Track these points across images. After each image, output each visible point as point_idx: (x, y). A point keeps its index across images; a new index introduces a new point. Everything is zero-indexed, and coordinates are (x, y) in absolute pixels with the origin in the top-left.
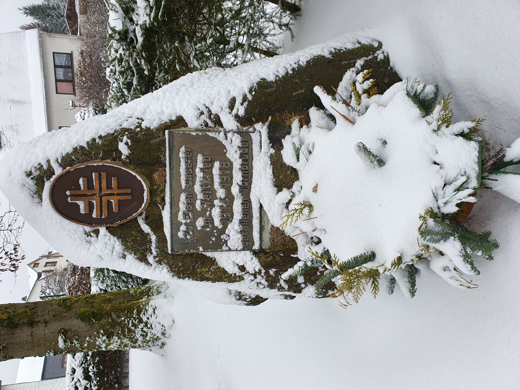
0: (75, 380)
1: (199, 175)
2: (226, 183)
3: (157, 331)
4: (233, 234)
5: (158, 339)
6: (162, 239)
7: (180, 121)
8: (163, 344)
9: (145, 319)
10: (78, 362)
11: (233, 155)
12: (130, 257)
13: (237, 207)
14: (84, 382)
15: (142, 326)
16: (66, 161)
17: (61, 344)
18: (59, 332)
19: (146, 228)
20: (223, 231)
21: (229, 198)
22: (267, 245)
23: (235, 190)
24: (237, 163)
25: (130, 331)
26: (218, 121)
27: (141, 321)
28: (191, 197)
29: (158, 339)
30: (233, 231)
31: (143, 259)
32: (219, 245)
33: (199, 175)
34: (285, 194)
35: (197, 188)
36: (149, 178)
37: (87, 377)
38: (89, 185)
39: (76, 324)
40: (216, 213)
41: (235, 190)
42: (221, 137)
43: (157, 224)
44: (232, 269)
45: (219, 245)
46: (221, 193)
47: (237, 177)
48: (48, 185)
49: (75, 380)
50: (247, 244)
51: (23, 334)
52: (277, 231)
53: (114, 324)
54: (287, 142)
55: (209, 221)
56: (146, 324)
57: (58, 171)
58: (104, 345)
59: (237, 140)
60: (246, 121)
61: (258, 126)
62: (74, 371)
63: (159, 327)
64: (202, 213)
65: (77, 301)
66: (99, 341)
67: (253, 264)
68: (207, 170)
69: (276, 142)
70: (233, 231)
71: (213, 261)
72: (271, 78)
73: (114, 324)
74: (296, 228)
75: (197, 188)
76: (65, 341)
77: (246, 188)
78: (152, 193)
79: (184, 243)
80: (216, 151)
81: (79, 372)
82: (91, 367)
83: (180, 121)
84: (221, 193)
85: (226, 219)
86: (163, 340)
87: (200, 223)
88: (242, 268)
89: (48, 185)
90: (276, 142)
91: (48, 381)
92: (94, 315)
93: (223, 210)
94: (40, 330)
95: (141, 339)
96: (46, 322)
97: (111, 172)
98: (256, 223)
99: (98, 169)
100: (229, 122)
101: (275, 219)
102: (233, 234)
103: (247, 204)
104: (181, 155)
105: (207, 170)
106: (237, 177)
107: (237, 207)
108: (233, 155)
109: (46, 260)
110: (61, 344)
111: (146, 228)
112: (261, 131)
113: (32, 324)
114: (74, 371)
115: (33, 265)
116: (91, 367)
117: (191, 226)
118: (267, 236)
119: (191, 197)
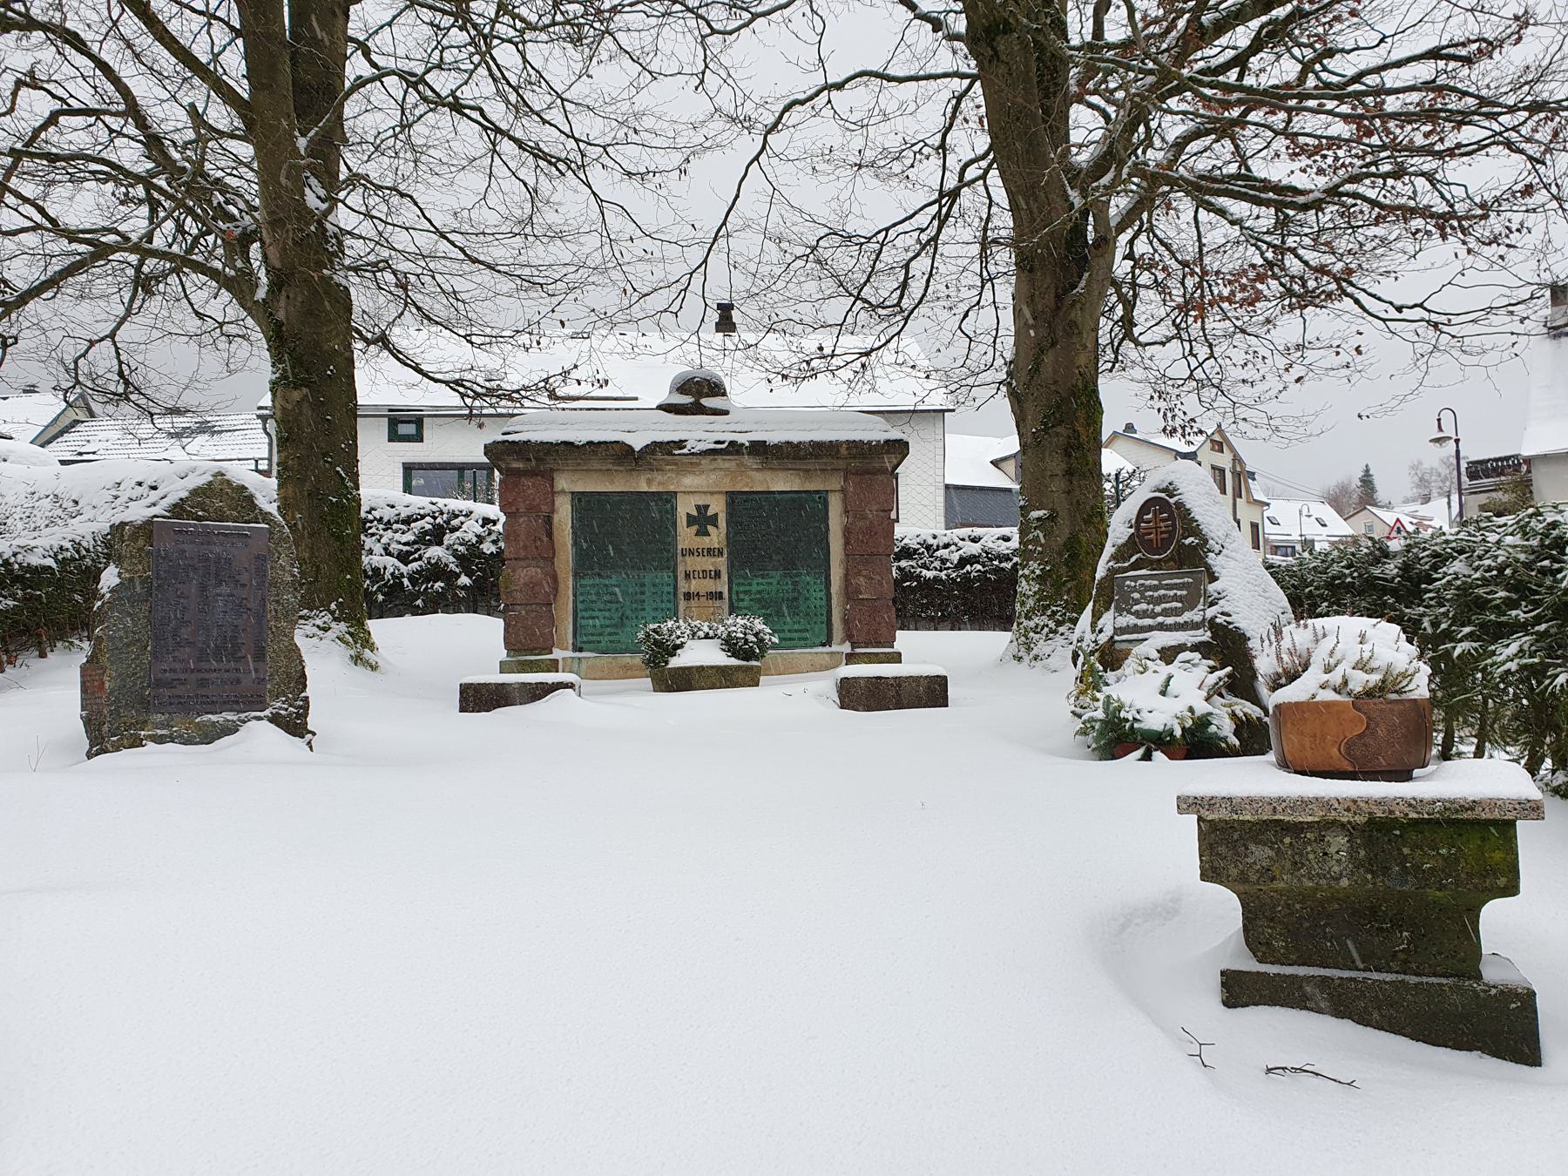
0: (961, 543)
1: (1172, 593)
2: (1165, 613)
3: (1042, 647)
4: (1127, 620)
5: (1029, 649)
6: (1126, 570)
7: (1213, 578)
8: (1020, 659)
9: (1061, 629)
10: (991, 545)
11: (1187, 617)
12: (1113, 550)
13: (1148, 622)
14: (955, 557)
15: (1052, 624)
16: (1179, 505)
17: (1035, 514)
18: (1053, 510)
19: (1133, 559)
20: (1129, 612)
21: (1154, 615)
22: (1117, 646)
23: (1160, 619)
24: (1180, 620)
25: (1046, 607)
26: (1212, 604)
27: (1059, 624)
28: (1155, 588)
29: (1029, 649)
30: (1131, 620)
31: (1114, 557)
32: (1119, 611)
33: (1172, 593)
34: (1156, 655)
35: (1162, 592)
36: (1166, 561)
37: (963, 562)
38: (1163, 520)
39: (1063, 533)
40: (1144, 606)
41: (1160, 619)
42: (1200, 607)
43: (1134, 567)
44: (1100, 624)
45: (1119, 611)
46: (1158, 609)
47: (1170, 620)
48: (1163, 495)
49: (961, 543)
50: (1119, 631)
51: (1056, 464)
52: (1127, 654)
53: (1058, 586)
54: (1197, 655)
55: (1137, 602)
56: (1055, 632)
57: (1172, 501)
58: (1026, 572)
59: (1198, 618)
60: (1212, 624)
61: (1209, 633)
62: (975, 540)
63: (1047, 650)
64: (1143, 597)
65: (1098, 530)
66: (1033, 565)
67: (1103, 639)
68: (1175, 598)
69: (1195, 648)
70: (1131, 620)
71: (1107, 609)
72: (1250, 644)
73: (1058, 586)
74: (1130, 665)
75: (1162, 592)
76: (1038, 519)
77: (1162, 627)
78: (1159, 561)
79: (1121, 586)
80: (1190, 604)
81: (974, 549)
82: (979, 567)
83: (1213, 578)
84: (1158, 609)
85: (1138, 615)
86: (1027, 658)
87: (1136, 595)
88: (1101, 631)
89: (1163, 495)
90: (1195, 648)
91: (941, 499)
92: (1074, 556)
93: (1145, 611)
94: (1057, 486)
95: (1032, 624)
96: (1069, 493)
97: (1172, 534)
98: (1134, 636)
99: (1174, 525)
100: (1210, 612)
101: (1138, 650)
102: (1127, 620)
103: (1150, 628)
104: (315, 24)
105: (1175, 598)
106: (1170, 620)
107: (1148, 622)
108: (1187, 617)
109: (1228, 466)
110: (1035, 514)
111: (1133, 559)
112: (1204, 636)
113: (1069, 473)
114: (975, 540)
115: (1217, 438)
116: (979, 567)
117: (1134, 589)
118: (1124, 646)
119: (1155, 588)
